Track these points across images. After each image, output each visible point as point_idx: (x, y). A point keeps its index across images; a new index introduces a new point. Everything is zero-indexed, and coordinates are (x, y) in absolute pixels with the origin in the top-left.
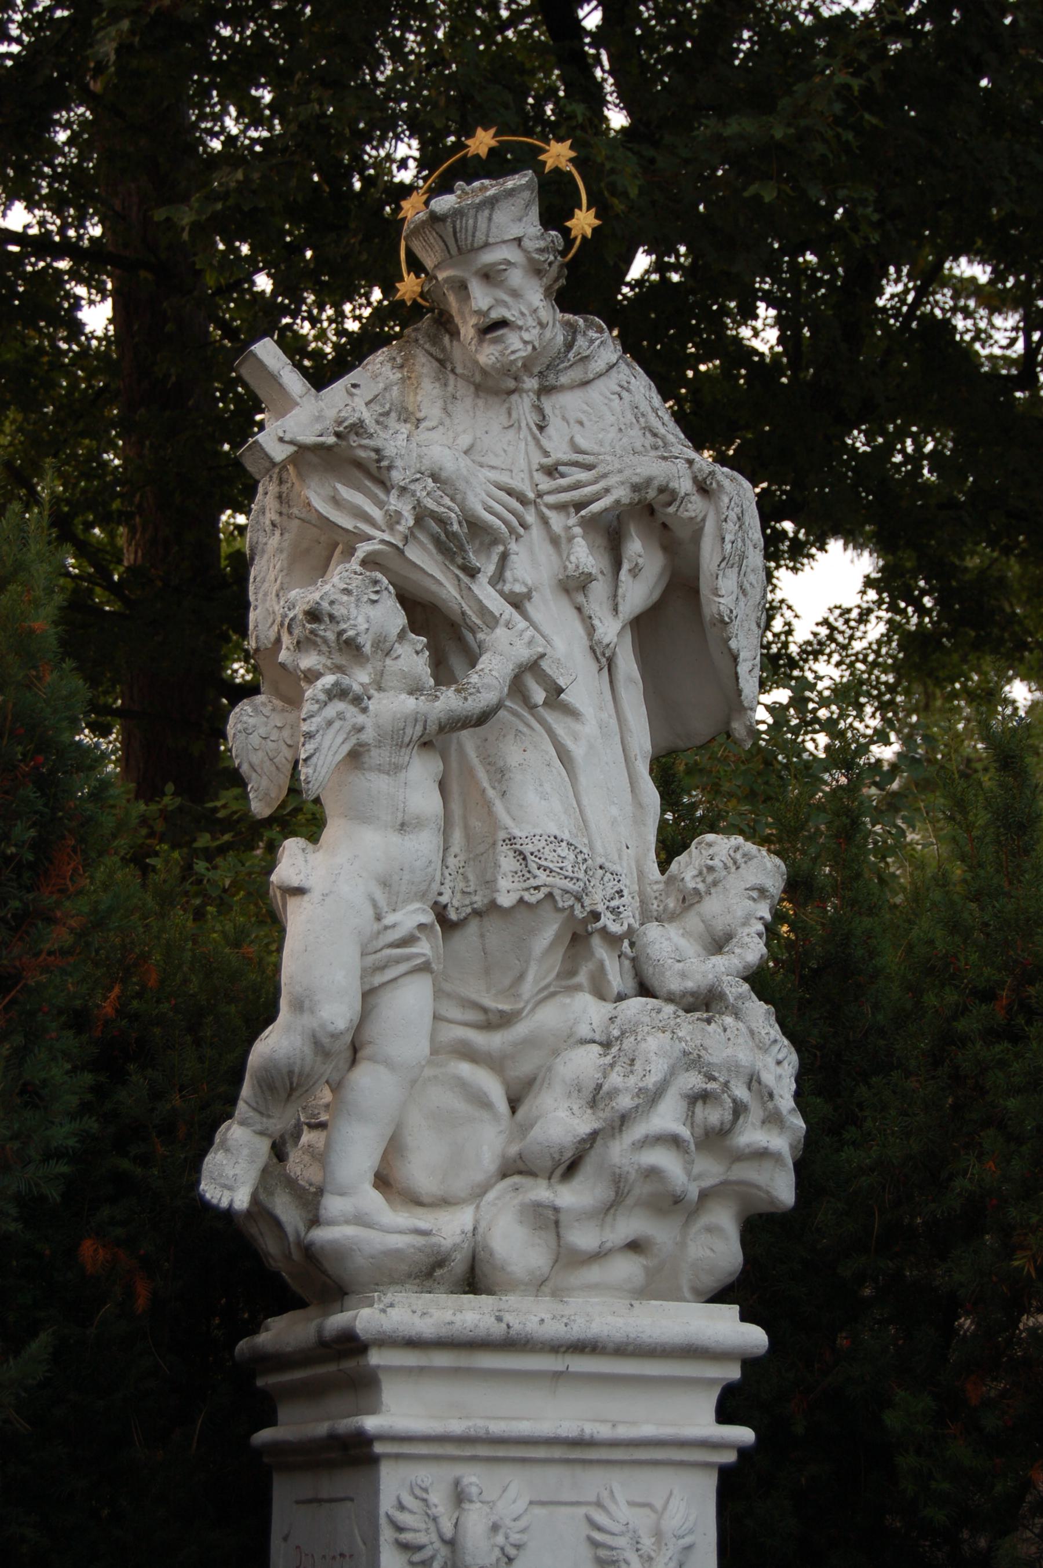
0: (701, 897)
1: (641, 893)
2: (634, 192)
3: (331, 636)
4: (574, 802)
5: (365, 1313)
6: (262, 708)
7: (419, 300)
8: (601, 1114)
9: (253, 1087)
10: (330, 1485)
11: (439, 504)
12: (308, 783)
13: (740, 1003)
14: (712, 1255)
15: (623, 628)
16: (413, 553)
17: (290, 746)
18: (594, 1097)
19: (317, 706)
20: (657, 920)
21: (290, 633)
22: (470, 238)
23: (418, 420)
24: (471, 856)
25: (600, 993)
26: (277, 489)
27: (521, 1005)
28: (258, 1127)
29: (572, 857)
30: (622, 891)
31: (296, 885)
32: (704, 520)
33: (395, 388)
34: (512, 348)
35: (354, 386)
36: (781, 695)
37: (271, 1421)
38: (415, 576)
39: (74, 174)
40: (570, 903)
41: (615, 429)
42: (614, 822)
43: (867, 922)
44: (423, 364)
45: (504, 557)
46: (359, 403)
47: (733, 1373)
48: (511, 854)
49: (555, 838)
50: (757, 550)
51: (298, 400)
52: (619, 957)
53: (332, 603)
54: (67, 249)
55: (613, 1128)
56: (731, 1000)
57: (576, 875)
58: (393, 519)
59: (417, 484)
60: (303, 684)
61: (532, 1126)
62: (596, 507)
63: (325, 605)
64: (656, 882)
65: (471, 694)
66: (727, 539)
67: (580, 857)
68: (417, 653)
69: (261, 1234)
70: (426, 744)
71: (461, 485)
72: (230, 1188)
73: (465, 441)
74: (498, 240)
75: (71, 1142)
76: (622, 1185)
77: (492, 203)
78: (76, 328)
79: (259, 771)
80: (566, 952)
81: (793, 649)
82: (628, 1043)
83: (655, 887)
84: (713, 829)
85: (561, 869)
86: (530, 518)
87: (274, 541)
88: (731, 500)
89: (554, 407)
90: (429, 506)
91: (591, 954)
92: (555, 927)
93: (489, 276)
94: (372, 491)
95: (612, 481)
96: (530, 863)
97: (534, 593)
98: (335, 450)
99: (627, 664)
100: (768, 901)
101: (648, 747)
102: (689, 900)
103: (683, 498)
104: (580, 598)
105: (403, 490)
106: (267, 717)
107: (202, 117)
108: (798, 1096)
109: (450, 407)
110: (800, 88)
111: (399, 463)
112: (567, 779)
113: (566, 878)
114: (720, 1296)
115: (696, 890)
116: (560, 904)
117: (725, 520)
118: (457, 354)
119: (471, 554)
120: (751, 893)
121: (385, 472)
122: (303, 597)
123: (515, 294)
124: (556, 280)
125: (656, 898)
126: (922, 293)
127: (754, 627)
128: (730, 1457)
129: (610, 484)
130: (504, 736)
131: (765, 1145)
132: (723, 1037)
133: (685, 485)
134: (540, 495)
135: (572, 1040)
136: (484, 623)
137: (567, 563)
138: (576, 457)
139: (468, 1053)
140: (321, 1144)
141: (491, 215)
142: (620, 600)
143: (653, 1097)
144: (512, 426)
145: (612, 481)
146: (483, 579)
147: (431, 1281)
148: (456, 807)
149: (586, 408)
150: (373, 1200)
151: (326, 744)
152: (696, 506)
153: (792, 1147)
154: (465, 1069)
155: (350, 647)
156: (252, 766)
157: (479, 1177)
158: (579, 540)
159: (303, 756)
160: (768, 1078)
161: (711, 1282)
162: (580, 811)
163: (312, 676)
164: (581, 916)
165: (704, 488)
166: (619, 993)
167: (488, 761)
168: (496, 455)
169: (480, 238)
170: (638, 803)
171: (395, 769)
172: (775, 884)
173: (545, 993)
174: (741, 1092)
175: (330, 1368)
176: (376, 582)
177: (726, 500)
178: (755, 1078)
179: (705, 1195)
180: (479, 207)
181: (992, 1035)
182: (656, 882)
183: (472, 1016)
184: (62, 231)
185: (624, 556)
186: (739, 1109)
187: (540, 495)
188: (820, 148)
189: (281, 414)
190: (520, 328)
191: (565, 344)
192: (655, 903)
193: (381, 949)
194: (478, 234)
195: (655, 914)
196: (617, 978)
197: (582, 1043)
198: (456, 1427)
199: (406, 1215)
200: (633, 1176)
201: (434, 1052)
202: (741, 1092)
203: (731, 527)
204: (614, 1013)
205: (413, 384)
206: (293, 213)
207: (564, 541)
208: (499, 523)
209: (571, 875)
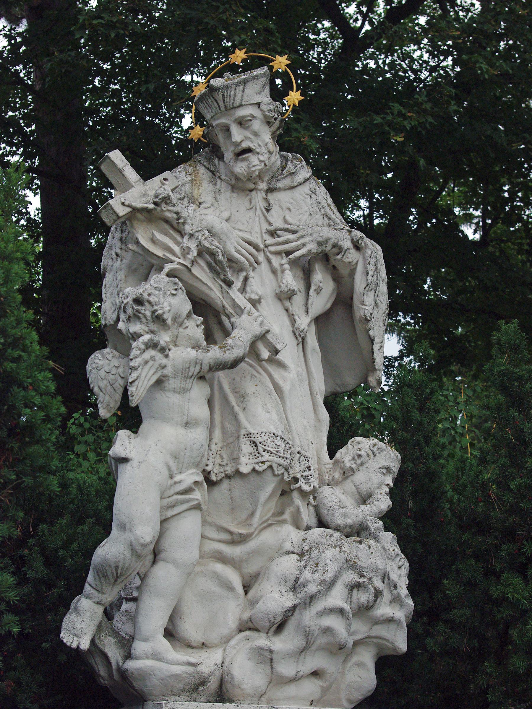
0: (354, 472)
1: (319, 470)
3: (148, 314)
4: (284, 416)
6: (107, 356)
7: (202, 139)
8: (299, 595)
9: (94, 576)
11: (212, 244)
12: (133, 396)
13: (378, 532)
14: (359, 680)
15: (311, 321)
16: (196, 271)
17: (122, 378)
18: (294, 585)
19: (139, 352)
20: (328, 485)
21: (125, 312)
22: (232, 101)
23: (200, 203)
24: (225, 444)
25: (297, 525)
26: (119, 235)
27: (252, 530)
28: (97, 600)
29: (283, 445)
30: (310, 467)
31: (123, 456)
32: (356, 264)
33: (187, 185)
34: (254, 164)
35: (165, 179)
40: (282, 472)
41: (307, 214)
42: (305, 427)
45: (246, 279)
48: (248, 443)
49: (274, 434)
50: (384, 283)
51: (133, 184)
52: (308, 505)
53: (149, 295)
55: (305, 604)
56: (373, 530)
57: (285, 456)
58: (186, 251)
59: (199, 233)
60: (131, 342)
61: (257, 602)
62: (297, 254)
63: (145, 295)
64: (328, 464)
65: (228, 349)
66: (370, 274)
67: (288, 446)
68: (197, 326)
69: (96, 664)
70: (202, 378)
71: (224, 237)
72: (76, 635)
73: (226, 215)
74: (247, 103)
76: (310, 637)
77: (245, 82)
79: (104, 392)
80: (277, 501)
83: (327, 466)
85: (277, 452)
88: (372, 253)
89: (274, 200)
90: (206, 245)
91: (293, 502)
92: (273, 485)
93: (242, 123)
94: (173, 236)
96: (259, 448)
97: (262, 300)
98: (153, 212)
99: (312, 341)
100: (392, 475)
101: (323, 388)
103: (346, 250)
104: (287, 304)
105: (191, 235)
106: (110, 361)
108: (409, 587)
109: (217, 196)
111: (189, 221)
112: (280, 402)
113: (280, 457)
115: (351, 469)
116: (276, 472)
117: (369, 264)
118: (222, 167)
119: (229, 274)
120: (382, 470)
121: (181, 226)
123: (256, 134)
124: (278, 129)
125: (327, 472)
127: (382, 325)
129: (305, 241)
130: (245, 377)
131: (392, 615)
132: (368, 552)
133: (347, 244)
134: (266, 247)
135: (281, 552)
136: (235, 312)
137: (281, 284)
138: (286, 226)
139: (222, 559)
140: (133, 611)
141: (244, 89)
142: (309, 306)
143: (330, 585)
144: (252, 208)
147: (196, 694)
149: (292, 201)
150: (164, 643)
151: (144, 374)
153: (406, 616)
154: (219, 567)
155: (159, 319)
156: (100, 388)
157: (226, 631)
158: (287, 271)
159: (130, 380)
160: (394, 576)
162: (287, 420)
163: (136, 336)
164: (287, 480)
165: (357, 247)
166: (307, 526)
167: (236, 391)
168: (243, 224)
171: (184, 391)
172: (395, 467)
173: (265, 524)
174: (378, 584)
176: (176, 284)
177: (370, 252)
178: (386, 576)
179: (356, 644)
180: (237, 84)
182: (328, 464)
185: (311, 282)
186: (378, 594)
187: (266, 247)
190: (258, 153)
191: (281, 167)
192: (327, 475)
193: (172, 495)
194: (236, 99)
195: (327, 481)
197: (286, 554)
199: (183, 653)
200: (316, 632)
201: (201, 557)
202: (378, 584)
203: (371, 267)
204: (305, 536)
205: (197, 184)
207: (279, 273)
208: (243, 259)
209: (283, 455)
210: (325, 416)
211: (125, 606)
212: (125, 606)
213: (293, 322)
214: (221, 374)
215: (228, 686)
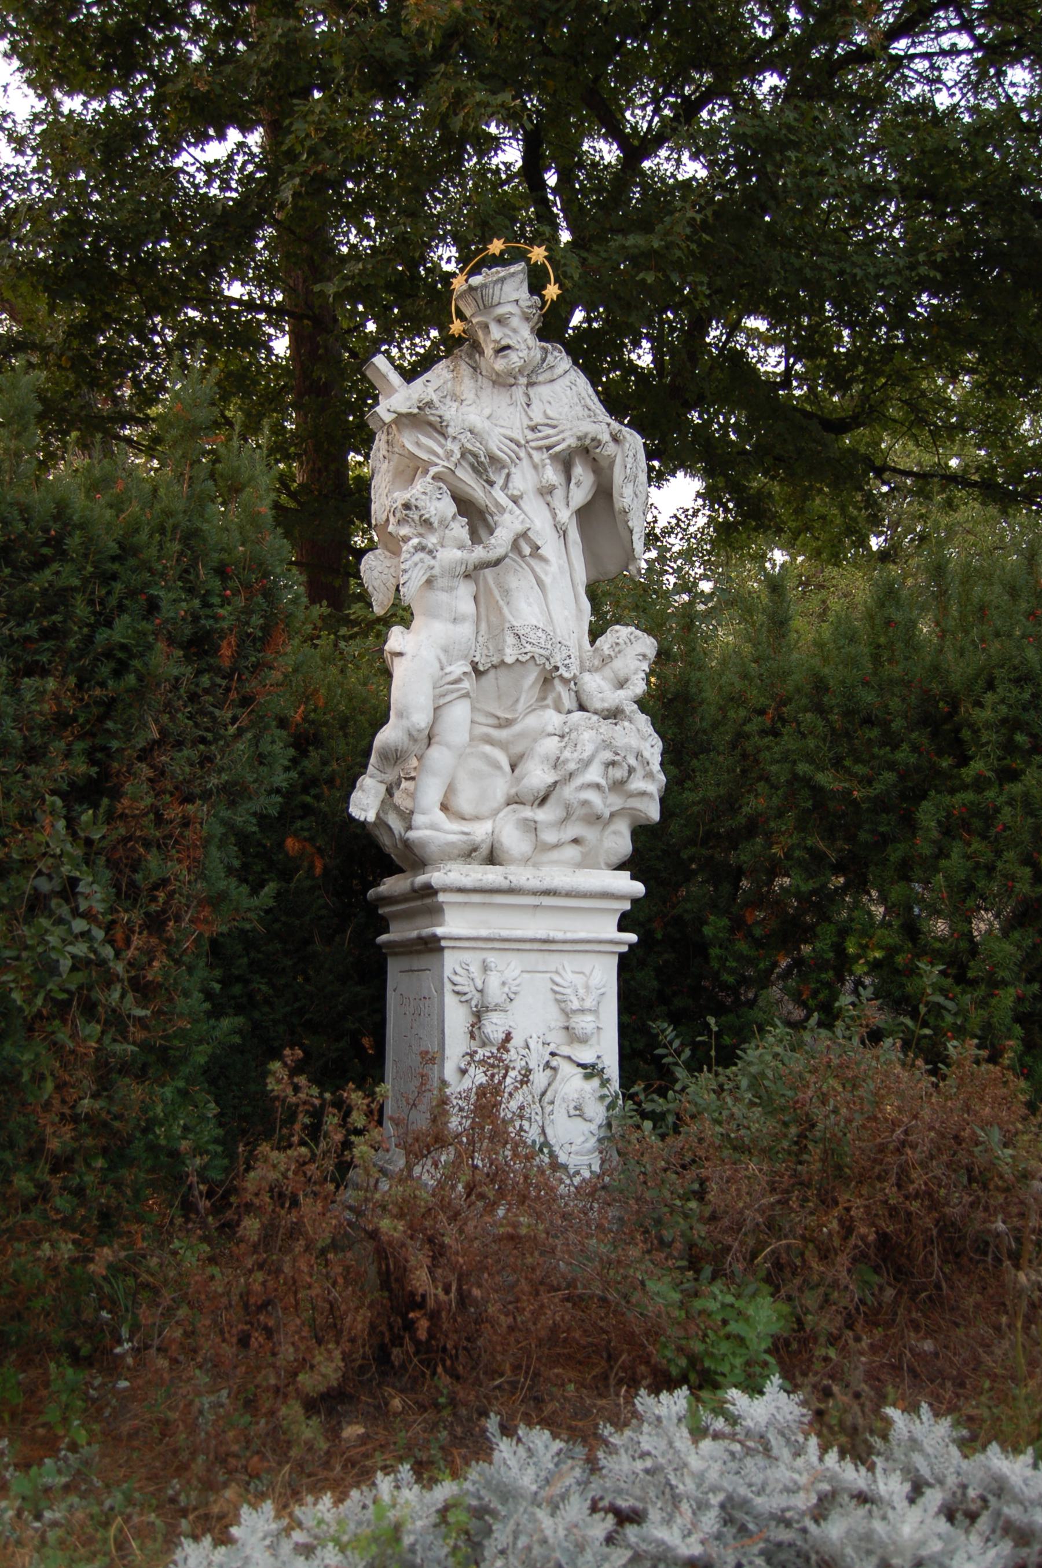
2: (576, 277)
5: (436, 874)
10: (418, 962)
16: (460, 473)
36: (653, 554)
37: (386, 930)
38: (461, 485)
39: (268, 264)
43: (698, 674)
44: (465, 369)
45: (508, 475)
46: (430, 390)
47: (627, 906)
54: (265, 308)
58: (449, 454)
62: (558, 449)
70: (467, 576)
73: (487, 412)
75: (285, 784)
77: (502, 280)
78: (270, 350)
81: (658, 531)
82: (574, 735)
84: (618, 623)
86: (522, 454)
87: (385, 466)
93: (500, 321)
95: (566, 434)
99: (574, 534)
102: (606, 660)
107: (337, 234)
110: (667, 219)
114: (621, 867)
118: (483, 364)
122: (401, 496)
123: (515, 331)
126: (730, 335)
128: (625, 949)
133: (606, 437)
143: (587, 764)
145: (566, 434)
146: (497, 487)
148: (482, 610)
150: (440, 816)
152: (611, 449)
154: (488, 749)
155: (427, 523)
157: (495, 805)
160: (646, 754)
161: (616, 860)
163: (406, 539)
167: (500, 586)
169: (496, 300)
170: (579, 610)
171: (451, 589)
172: (652, 653)
174: (632, 761)
175: (419, 903)
179: (612, 815)
180: (495, 282)
181: (763, 733)
183: (492, 721)
184: (261, 298)
186: (631, 770)
188: (678, 253)
189: (389, 397)
196: (568, 701)
198: (484, 933)
201: (472, 739)
202: (632, 761)
203: (630, 460)
206: (389, 288)
210: (586, 605)
211: (404, 784)
212: (404, 784)
213: (554, 516)
214: (487, 571)
215: (496, 853)
